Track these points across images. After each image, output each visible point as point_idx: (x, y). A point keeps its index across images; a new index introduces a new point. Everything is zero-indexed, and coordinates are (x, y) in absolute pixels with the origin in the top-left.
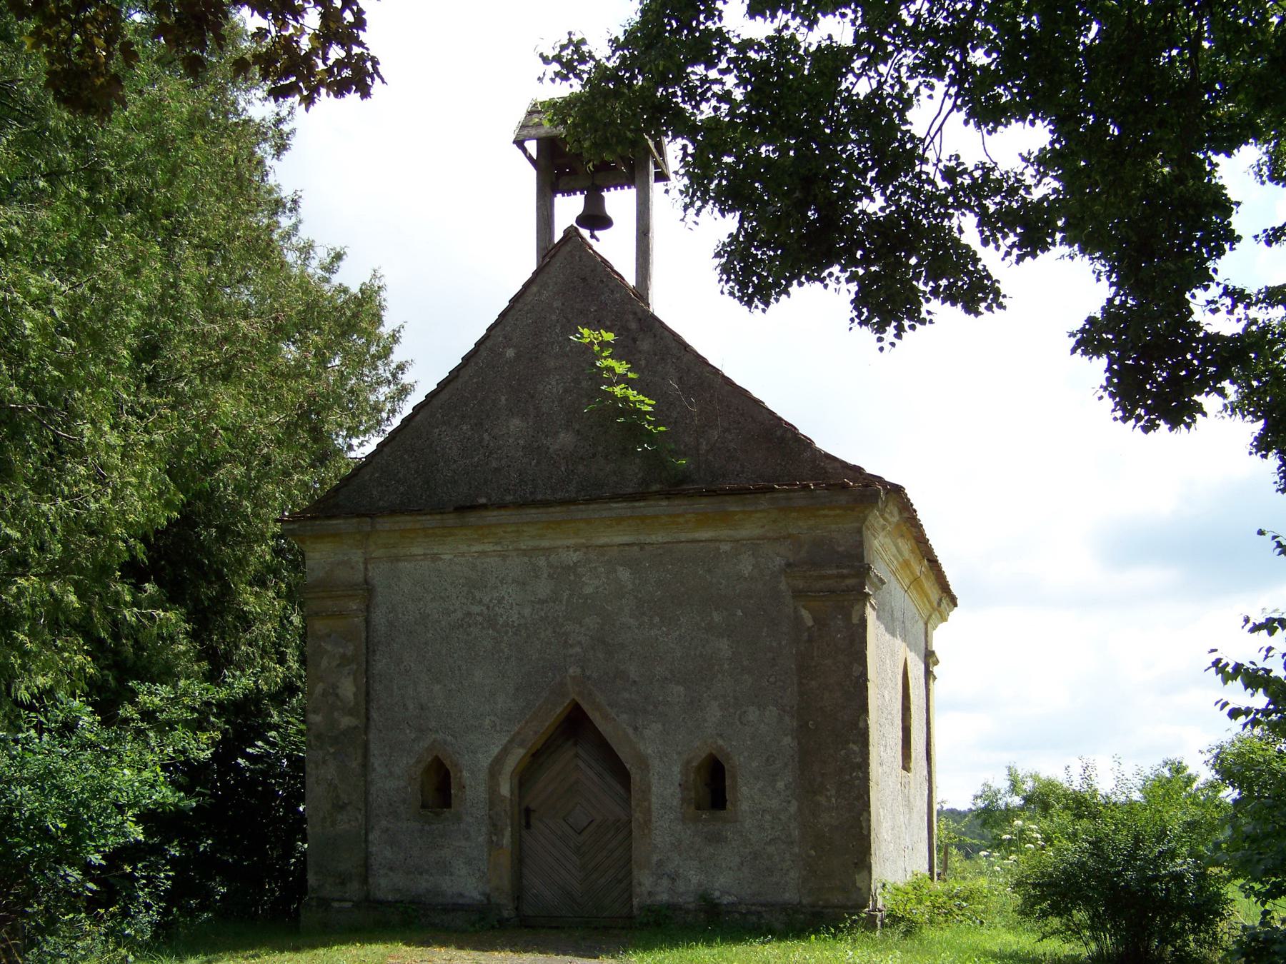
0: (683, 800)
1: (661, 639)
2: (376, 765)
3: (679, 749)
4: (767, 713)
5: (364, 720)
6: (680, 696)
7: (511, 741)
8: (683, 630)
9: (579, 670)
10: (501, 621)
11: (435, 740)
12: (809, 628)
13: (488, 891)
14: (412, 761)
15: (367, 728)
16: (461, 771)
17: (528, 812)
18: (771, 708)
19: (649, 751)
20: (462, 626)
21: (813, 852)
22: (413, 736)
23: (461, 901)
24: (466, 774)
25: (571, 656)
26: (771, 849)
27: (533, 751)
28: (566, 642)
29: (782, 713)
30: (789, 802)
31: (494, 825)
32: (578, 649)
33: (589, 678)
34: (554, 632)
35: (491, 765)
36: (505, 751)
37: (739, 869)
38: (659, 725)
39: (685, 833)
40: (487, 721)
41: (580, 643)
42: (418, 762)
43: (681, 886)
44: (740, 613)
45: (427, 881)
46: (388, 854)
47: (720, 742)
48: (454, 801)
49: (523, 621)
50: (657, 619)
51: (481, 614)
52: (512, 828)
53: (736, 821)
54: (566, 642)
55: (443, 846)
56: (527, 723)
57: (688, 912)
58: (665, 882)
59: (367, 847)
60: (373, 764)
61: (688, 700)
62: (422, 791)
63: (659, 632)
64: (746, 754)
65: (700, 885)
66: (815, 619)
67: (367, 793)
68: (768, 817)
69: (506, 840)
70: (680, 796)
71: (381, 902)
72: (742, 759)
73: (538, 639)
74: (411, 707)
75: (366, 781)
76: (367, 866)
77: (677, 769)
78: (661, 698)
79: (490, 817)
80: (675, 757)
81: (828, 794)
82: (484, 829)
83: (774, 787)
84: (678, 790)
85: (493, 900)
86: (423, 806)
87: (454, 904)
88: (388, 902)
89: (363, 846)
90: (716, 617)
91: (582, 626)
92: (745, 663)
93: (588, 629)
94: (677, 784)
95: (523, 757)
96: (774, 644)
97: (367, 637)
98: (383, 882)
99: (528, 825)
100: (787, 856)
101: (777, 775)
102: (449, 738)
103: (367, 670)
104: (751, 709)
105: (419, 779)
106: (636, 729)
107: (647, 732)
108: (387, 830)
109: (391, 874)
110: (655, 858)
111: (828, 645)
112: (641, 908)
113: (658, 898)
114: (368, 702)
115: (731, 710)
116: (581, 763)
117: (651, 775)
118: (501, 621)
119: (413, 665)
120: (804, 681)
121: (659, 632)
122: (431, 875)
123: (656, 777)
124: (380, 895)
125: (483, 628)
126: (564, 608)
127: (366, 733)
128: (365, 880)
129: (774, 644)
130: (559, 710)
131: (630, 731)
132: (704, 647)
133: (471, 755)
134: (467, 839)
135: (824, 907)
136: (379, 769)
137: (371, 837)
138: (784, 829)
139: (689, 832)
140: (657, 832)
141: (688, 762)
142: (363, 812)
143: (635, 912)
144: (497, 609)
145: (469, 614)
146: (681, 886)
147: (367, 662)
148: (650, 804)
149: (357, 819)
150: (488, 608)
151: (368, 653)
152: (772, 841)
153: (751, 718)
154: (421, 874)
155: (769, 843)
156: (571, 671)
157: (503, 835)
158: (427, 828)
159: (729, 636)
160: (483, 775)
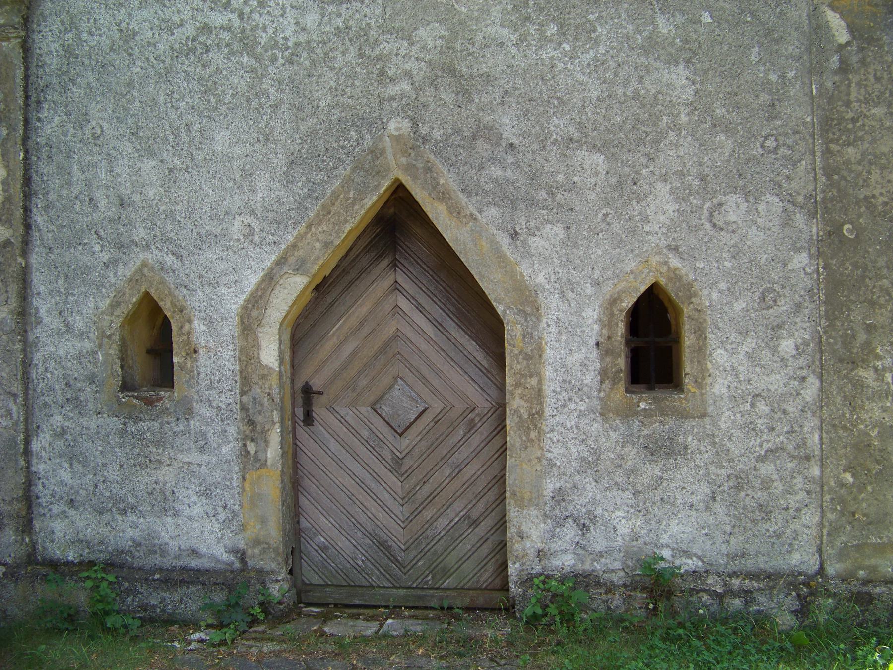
0: (603, 374)
1: (560, 66)
2: (43, 312)
3: (597, 274)
4: (762, 207)
5: (21, 230)
6: (596, 174)
7: (281, 262)
8: (602, 49)
9: (406, 125)
10: (264, 38)
11: (144, 264)
12: (841, 47)
13: (242, 545)
14: (104, 304)
15: (26, 243)
16: (190, 321)
17: (308, 393)
18: (770, 197)
19: (541, 279)
20: (193, 50)
21: (848, 478)
22: (105, 257)
23: (194, 563)
24: (199, 326)
25: (393, 98)
26: (767, 469)
27: (319, 280)
28: (382, 73)
29: (790, 208)
30: (803, 379)
31: (251, 423)
32: (405, 86)
33: (425, 140)
34: (361, 55)
35: (244, 308)
36: (270, 280)
37: (708, 508)
38: (559, 230)
39: (608, 437)
40: (237, 224)
41: (408, 75)
42: (115, 305)
43: (598, 540)
44: (707, 18)
45: (134, 526)
46: (66, 476)
47: (675, 262)
48: (179, 377)
49: (303, 38)
50: (552, 29)
51: (228, 29)
52: (282, 427)
53: (704, 416)
54: (382, 73)
55: (160, 462)
56: (309, 227)
57: (610, 588)
58: (569, 532)
59: (29, 465)
60: (37, 309)
61: (613, 181)
62: (122, 359)
63: (557, 54)
64: (723, 286)
65: (635, 537)
66: (851, 29)
67: (27, 365)
68: (762, 407)
69: (273, 451)
70: (598, 366)
71: (54, 565)
72: (715, 295)
73: (332, 69)
74: (103, 203)
75: (25, 342)
76: (29, 499)
77: (592, 314)
78: (560, 177)
79: (243, 408)
80: (589, 290)
81: (879, 364)
82: (232, 430)
83: (775, 351)
84: (594, 354)
85: (250, 563)
86: (125, 387)
87: (184, 569)
88: (68, 563)
89: (22, 463)
90: (664, 26)
91: (412, 44)
92: (720, 112)
93: (424, 48)
94: (592, 342)
95: (302, 292)
96: (773, 77)
97: (26, 77)
98: (59, 527)
99: (308, 419)
100: (798, 481)
101: (780, 326)
102: (169, 259)
103: (26, 139)
104: (732, 199)
105: (116, 338)
106: (514, 235)
107: (536, 243)
108: (63, 432)
109: (72, 512)
110: (550, 487)
111: (878, 79)
112: (527, 581)
113: (556, 562)
114: (27, 196)
115: (696, 201)
116: (403, 303)
117: (543, 325)
118: (264, 38)
119: (106, 126)
120: (834, 147)
121: (557, 54)
122: (142, 514)
123: (553, 329)
124: (55, 551)
125: (231, 53)
126: (377, 12)
127: (25, 253)
128: (26, 525)
129: (773, 77)
130: (371, 201)
131: (504, 240)
132: (641, 80)
133: (208, 290)
134: (202, 449)
135: (866, 582)
136: (46, 320)
137: (35, 445)
138: (792, 432)
139: (614, 435)
140: (555, 436)
141: (614, 301)
142: (20, 400)
143: (515, 589)
144: (256, 16)
145: (206, 29)
146: (598, 540)
147: (26, 122)
148: (540, 382)
149: (9, 413)
150: (241, 16)
151: (27, 105)
152: (773, 453)
153: (732, 217)
154: (123, 512)
155: (762, 459)
156: (392, 126)
157: (267, 442)
158: (131, 427)
159: (688, 61)
160: (230, 328)
